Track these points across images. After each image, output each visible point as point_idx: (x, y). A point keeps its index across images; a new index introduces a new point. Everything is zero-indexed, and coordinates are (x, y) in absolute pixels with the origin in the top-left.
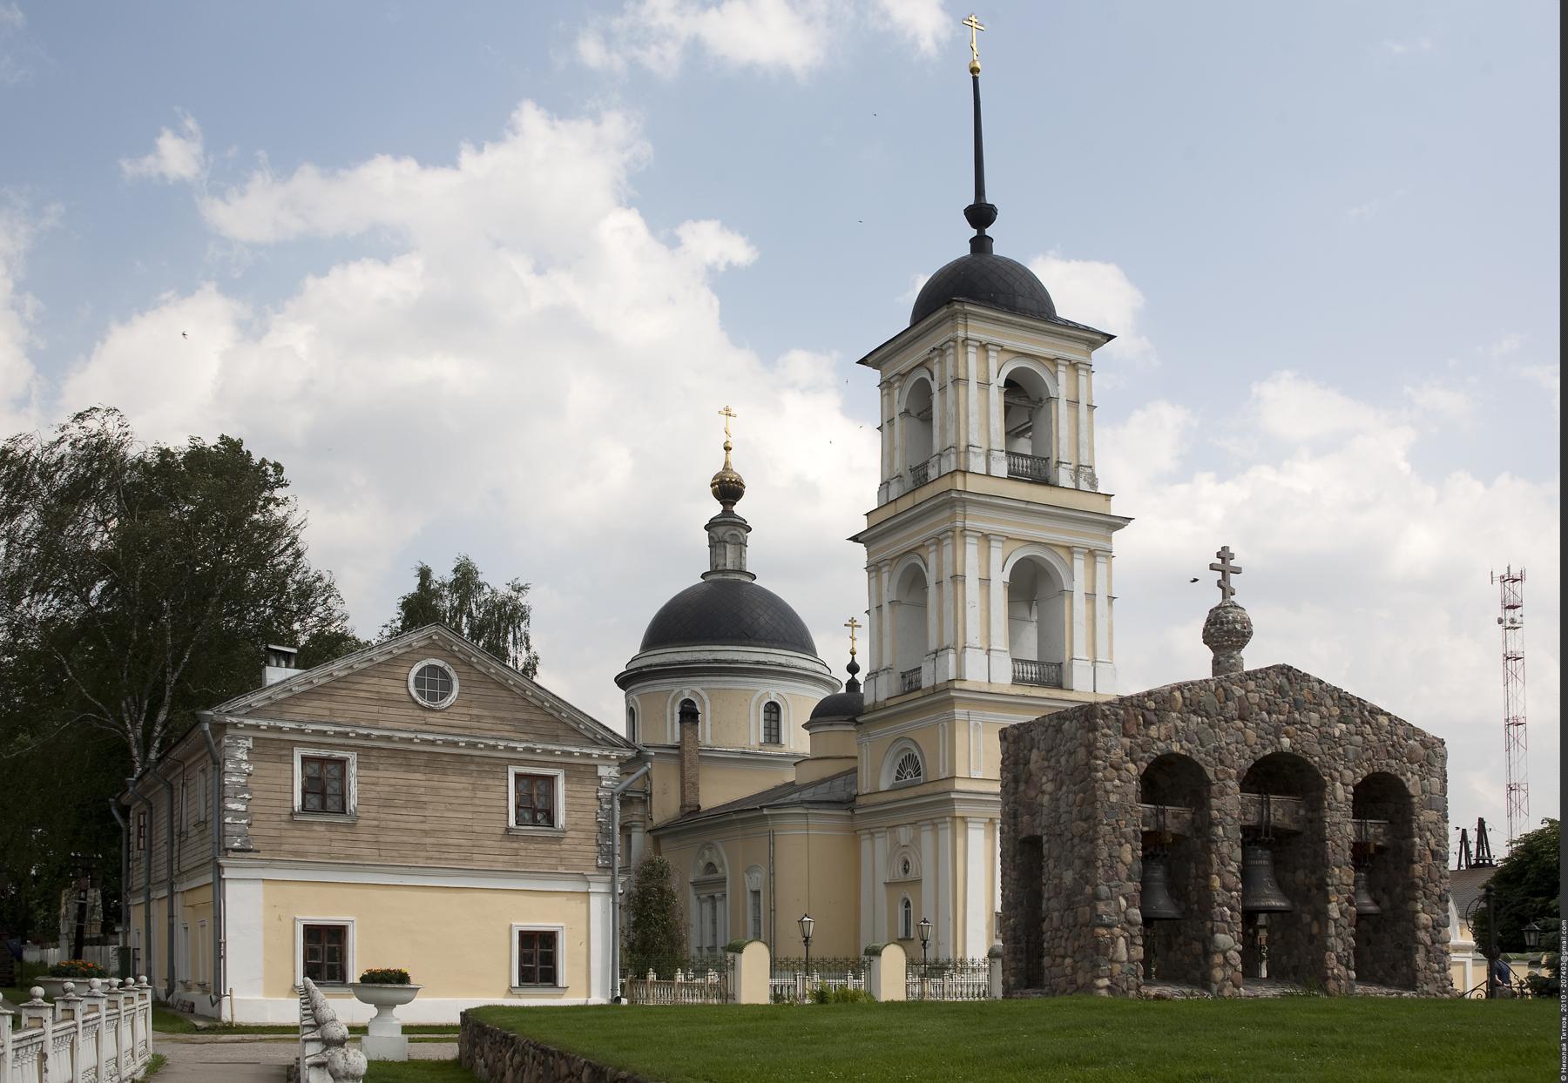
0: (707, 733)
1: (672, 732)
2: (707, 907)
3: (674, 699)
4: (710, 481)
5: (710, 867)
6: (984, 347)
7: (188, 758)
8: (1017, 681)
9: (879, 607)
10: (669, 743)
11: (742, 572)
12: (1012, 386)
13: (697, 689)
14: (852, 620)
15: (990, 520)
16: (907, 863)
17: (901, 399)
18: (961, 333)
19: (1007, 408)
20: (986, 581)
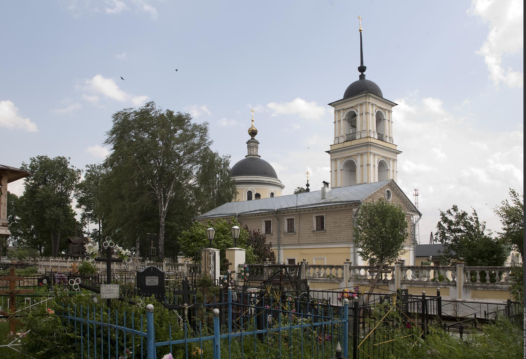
3: (246, 190)
7: (413, 285)
9: (336, 171)
18: (368, 101)
20: (374, 166)
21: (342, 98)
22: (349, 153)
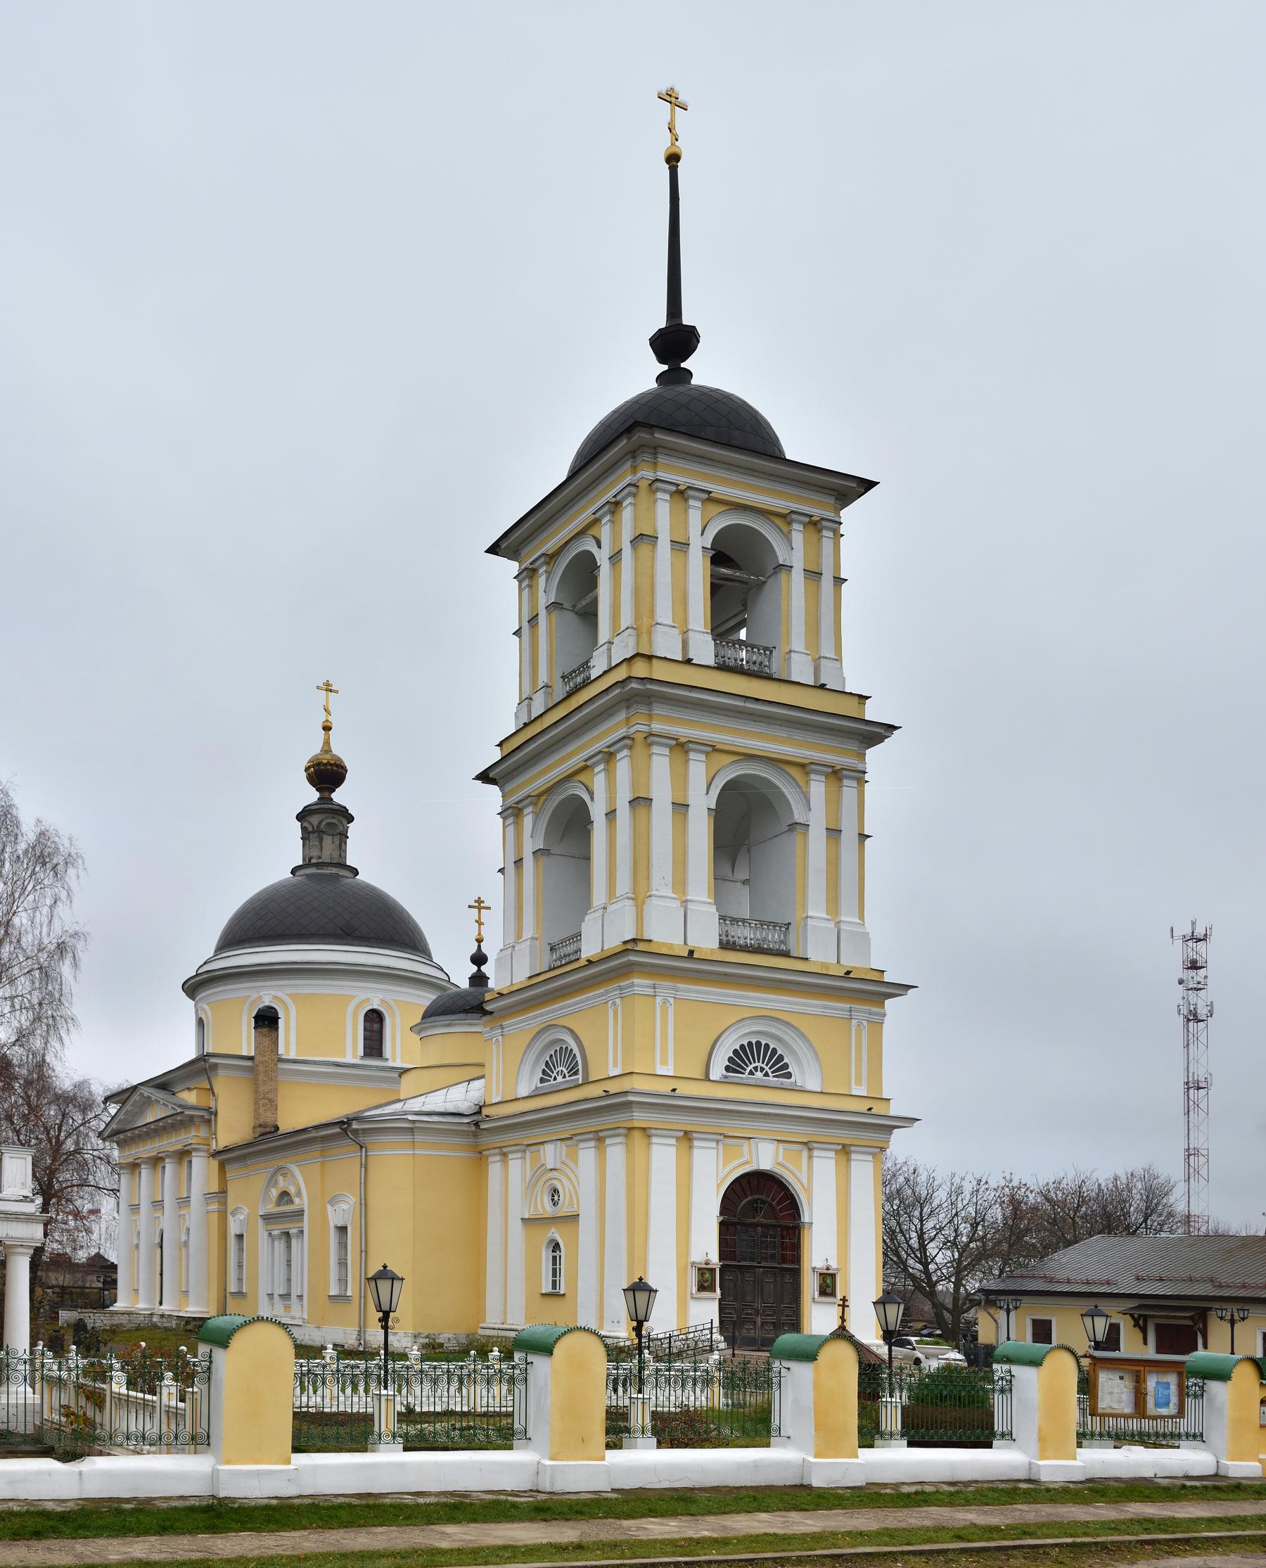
0: (289, 1042)
1: (245, 1041)
2: (280, 1246)
5: (285, 1196)
6: (681, 494)
8: (726, 945)
9: (519, 862)
10: (245, 1053)
11: (344, 866)
12: (719, 557)
13: (280, 994)
14: (479, 901)
15: (682, 722)
16: (556, 1191)
17: (546, 589)
19: (715, 589)
20: (681, 808)
22: (546, 771)
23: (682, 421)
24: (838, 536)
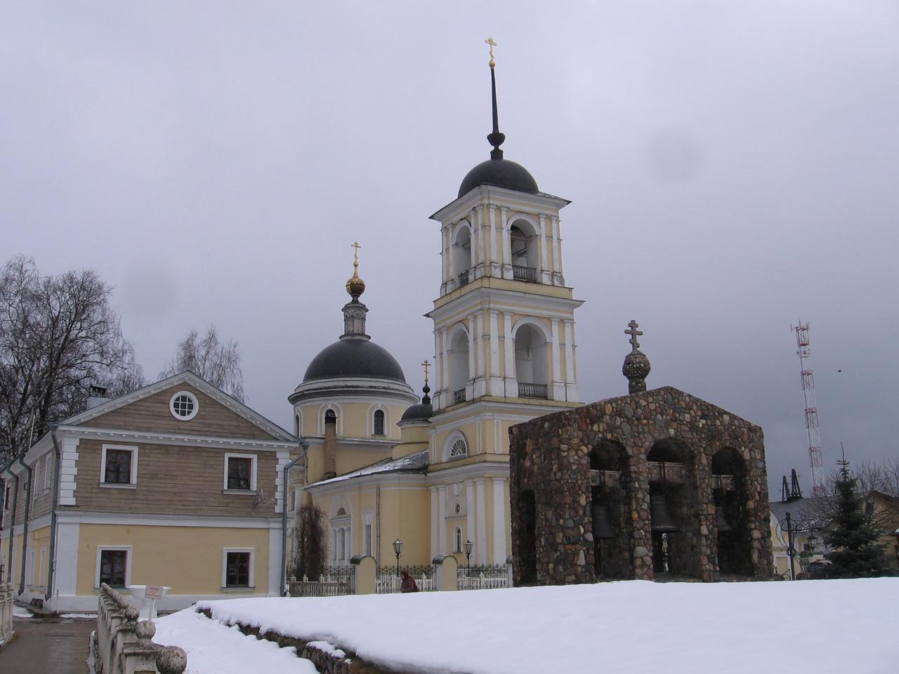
1: (320, 429)
4: (345, 283)
6: (499, 208)
8: (520, 395)
9: (441, 354)
11: (363, 334)
13: (336, 403)
20: (502, 338)
21: (457, 198)
23: (498, 175)
24: (558, 221)
